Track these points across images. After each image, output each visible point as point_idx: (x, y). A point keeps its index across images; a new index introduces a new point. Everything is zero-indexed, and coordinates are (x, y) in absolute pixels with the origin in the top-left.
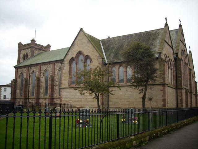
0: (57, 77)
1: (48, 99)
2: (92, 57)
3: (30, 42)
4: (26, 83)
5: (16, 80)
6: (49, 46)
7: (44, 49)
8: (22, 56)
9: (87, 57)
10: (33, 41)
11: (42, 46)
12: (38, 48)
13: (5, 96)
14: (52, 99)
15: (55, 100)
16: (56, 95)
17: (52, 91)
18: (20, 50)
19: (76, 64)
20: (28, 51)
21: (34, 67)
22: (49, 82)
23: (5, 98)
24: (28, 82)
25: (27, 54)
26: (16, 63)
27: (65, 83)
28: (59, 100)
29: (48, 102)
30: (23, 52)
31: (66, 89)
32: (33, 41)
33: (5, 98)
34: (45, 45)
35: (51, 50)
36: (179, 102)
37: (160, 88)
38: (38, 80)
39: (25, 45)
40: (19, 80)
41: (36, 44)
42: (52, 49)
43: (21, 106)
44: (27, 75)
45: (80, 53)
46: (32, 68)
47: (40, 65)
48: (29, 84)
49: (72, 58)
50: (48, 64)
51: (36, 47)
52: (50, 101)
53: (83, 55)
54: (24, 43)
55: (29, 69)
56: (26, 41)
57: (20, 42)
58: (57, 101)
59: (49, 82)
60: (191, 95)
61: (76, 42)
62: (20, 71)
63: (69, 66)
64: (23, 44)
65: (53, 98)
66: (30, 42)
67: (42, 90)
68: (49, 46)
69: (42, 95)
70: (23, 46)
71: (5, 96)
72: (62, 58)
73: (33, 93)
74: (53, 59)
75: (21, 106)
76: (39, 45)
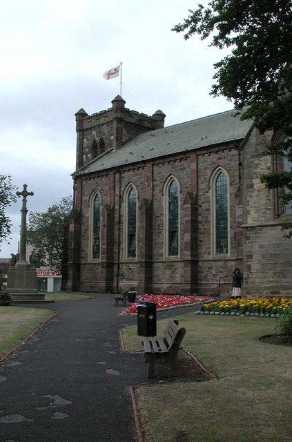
1: (180, 264)
3: (111, 106)
5: (81, 212)
6: (160, 116)
11: (143, 117)
18: (81, 130)
21: (131, 173)
24: (117, 215)
26: (72, 167)
34: (150, 112)
35: (165, 125)
38: (149, 210)
41: (127, 111)
42: (168, 123)
46: (126, 175)
47: (149, 165)
50: (86, 179)
55: (117, 179)
56: (98, 105)
57: (82, 109)
59: (103, 220)
62: (89, 185)
64: (90, 114)
66: (111, 106)
68: (160, 116)
70: (90, 117)
73: (96, 247)
74: (231, 133)
76: (134, 113)
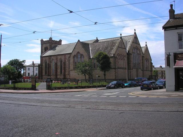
0: (67, 63)
2: (84, 55)
4: (48, 66)
7: (57, 43)
8: (43, 48)
9: (82, 55)
10: (51, 39)
12: (54, 42)
13: (29, 73)
14: (65, 75)
15: (67, 76)
16: (67, 73)
17: (65, 71)
19: (77, 58)
20: (48, 45)
22: (63, 66)
23: (29, 75)
25: (47, 47)
27: (72, 67)
28: (69, 76)
29: (62, 77)
30: (44, 46)
31: (26, 94)
32: (51, 39)
33: (29, 75)
36: (129, 76)
37: (114, 70)
38: (56, 64)
39: (46, 41)
40: (44, 64)
42: (63, 43)
43: (89, 68)
44: (49, 61)
45: (78, 52)
46: (52, 57)
48: (51, 67)
49: (75, 55)
51: (53, 42)
52: (64, 77)
53: (80, 54)
54: (44, 40)
58: (68, 77)
60: (143, 72)
61: (76, 47)
63: (73, 59)
65: (57, 75)
67: (59, 70)
68: (60, 41)
69: (59, 73)
71: (29, 73)
72: (71, 52)
75: (89, 68)
